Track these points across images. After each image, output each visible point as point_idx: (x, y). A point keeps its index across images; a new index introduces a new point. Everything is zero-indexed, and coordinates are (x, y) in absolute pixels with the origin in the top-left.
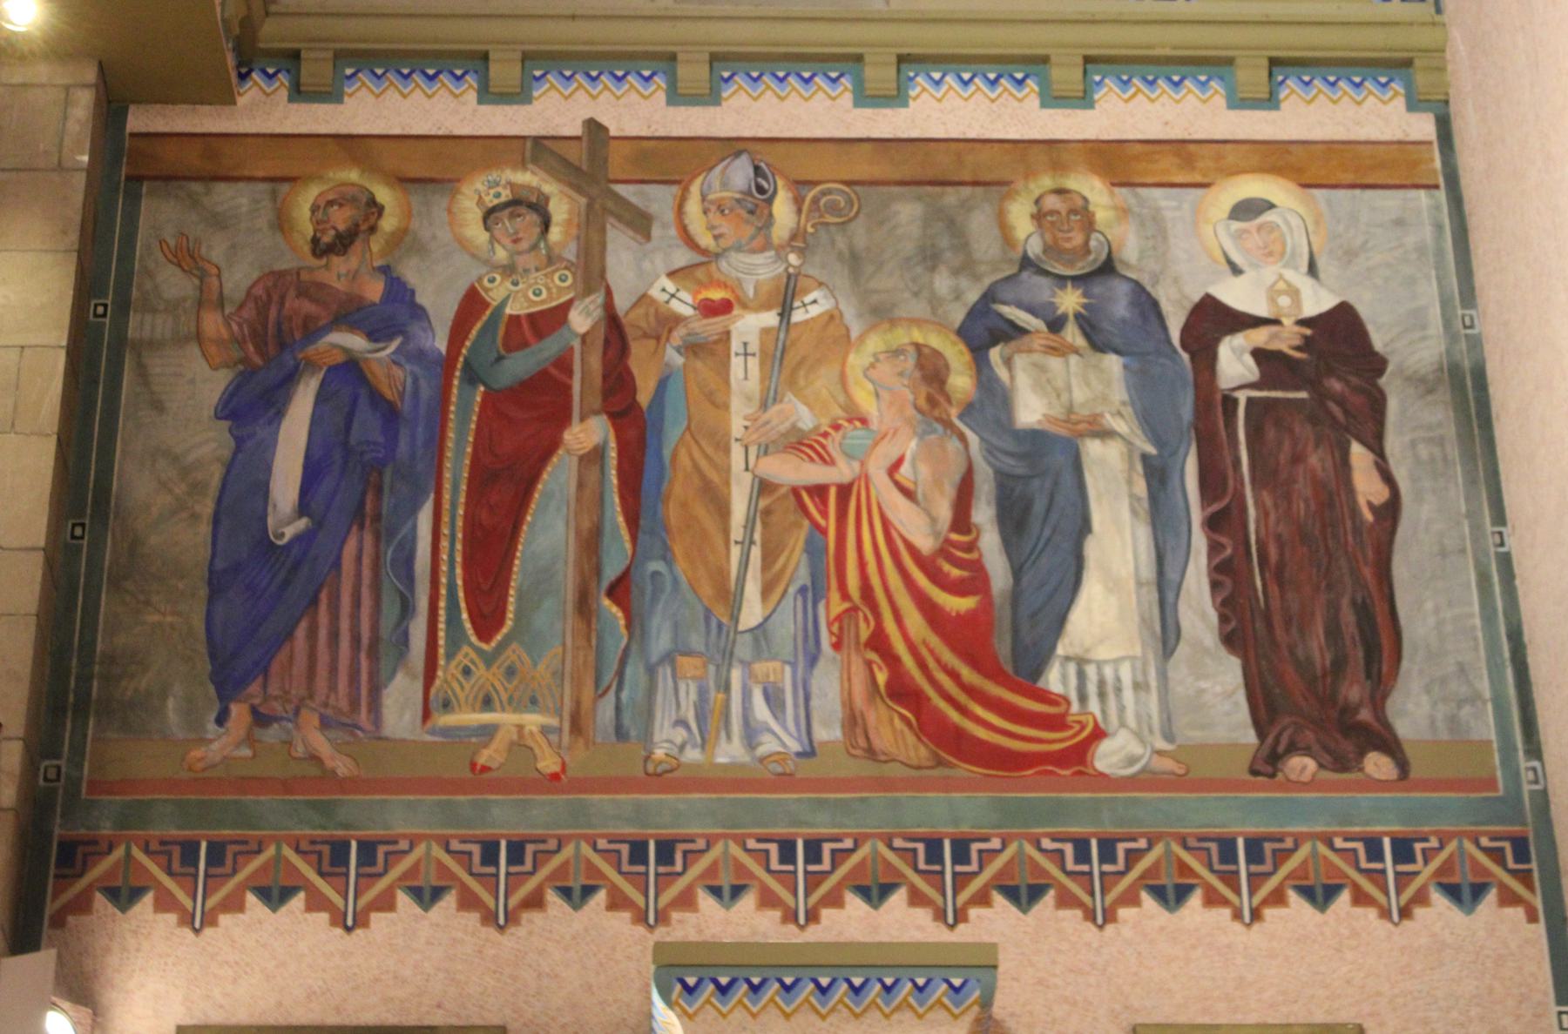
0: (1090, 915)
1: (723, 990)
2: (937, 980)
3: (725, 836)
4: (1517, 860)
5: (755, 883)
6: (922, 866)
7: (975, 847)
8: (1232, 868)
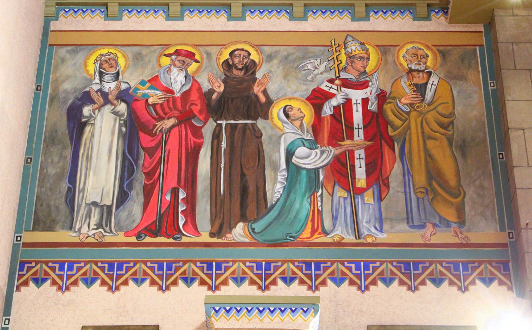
0: (360, 288)
1: (228, 311)
2: (255, 308)
3: (239, 261)
4: (455, 270)
5: (448, 277)
6: (403, 271)
7: (470, 266)
8: (458, 273)
